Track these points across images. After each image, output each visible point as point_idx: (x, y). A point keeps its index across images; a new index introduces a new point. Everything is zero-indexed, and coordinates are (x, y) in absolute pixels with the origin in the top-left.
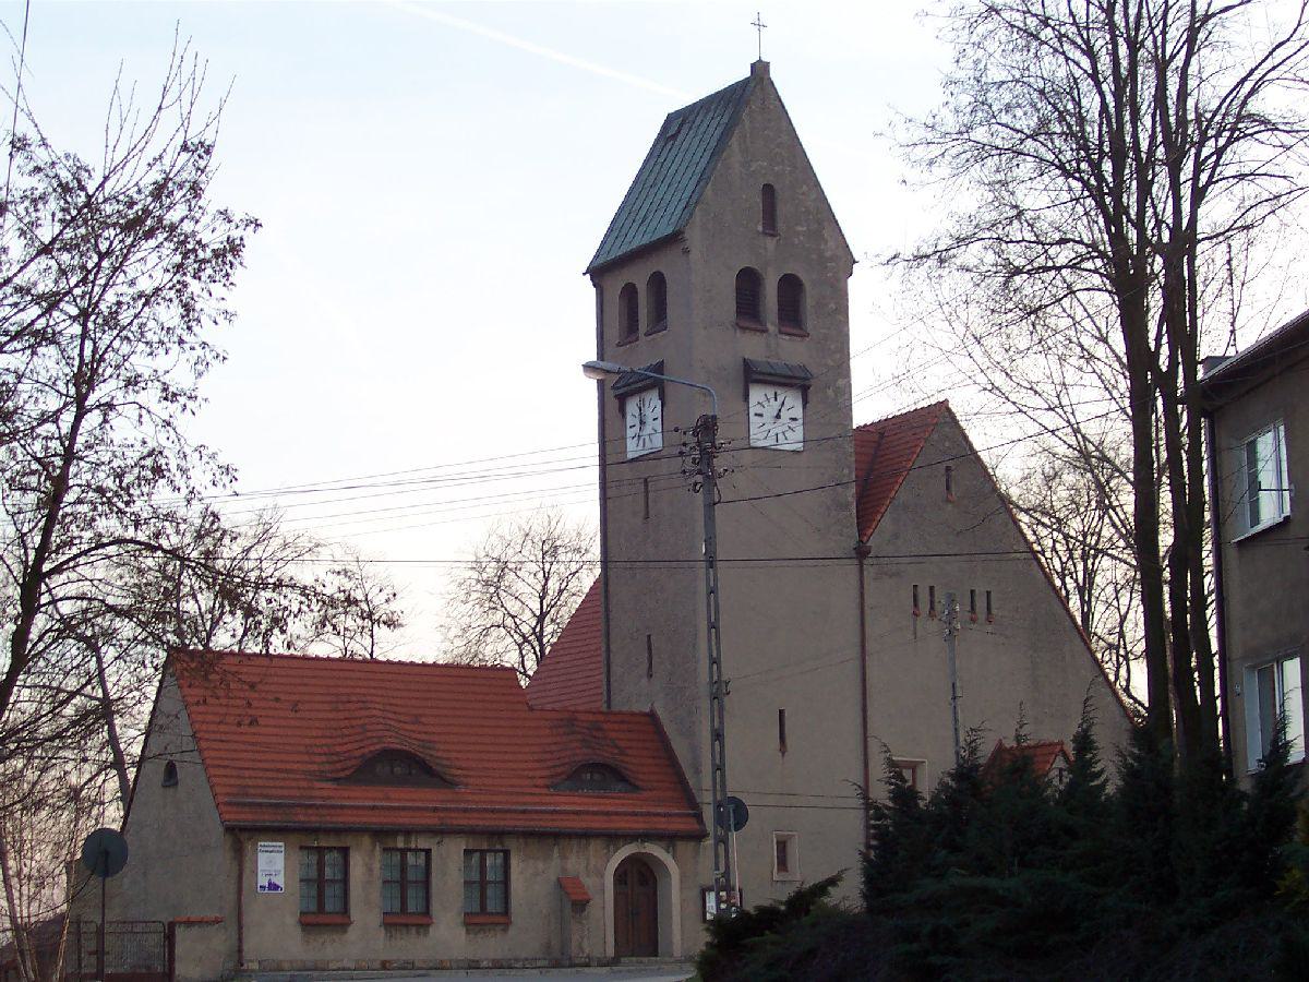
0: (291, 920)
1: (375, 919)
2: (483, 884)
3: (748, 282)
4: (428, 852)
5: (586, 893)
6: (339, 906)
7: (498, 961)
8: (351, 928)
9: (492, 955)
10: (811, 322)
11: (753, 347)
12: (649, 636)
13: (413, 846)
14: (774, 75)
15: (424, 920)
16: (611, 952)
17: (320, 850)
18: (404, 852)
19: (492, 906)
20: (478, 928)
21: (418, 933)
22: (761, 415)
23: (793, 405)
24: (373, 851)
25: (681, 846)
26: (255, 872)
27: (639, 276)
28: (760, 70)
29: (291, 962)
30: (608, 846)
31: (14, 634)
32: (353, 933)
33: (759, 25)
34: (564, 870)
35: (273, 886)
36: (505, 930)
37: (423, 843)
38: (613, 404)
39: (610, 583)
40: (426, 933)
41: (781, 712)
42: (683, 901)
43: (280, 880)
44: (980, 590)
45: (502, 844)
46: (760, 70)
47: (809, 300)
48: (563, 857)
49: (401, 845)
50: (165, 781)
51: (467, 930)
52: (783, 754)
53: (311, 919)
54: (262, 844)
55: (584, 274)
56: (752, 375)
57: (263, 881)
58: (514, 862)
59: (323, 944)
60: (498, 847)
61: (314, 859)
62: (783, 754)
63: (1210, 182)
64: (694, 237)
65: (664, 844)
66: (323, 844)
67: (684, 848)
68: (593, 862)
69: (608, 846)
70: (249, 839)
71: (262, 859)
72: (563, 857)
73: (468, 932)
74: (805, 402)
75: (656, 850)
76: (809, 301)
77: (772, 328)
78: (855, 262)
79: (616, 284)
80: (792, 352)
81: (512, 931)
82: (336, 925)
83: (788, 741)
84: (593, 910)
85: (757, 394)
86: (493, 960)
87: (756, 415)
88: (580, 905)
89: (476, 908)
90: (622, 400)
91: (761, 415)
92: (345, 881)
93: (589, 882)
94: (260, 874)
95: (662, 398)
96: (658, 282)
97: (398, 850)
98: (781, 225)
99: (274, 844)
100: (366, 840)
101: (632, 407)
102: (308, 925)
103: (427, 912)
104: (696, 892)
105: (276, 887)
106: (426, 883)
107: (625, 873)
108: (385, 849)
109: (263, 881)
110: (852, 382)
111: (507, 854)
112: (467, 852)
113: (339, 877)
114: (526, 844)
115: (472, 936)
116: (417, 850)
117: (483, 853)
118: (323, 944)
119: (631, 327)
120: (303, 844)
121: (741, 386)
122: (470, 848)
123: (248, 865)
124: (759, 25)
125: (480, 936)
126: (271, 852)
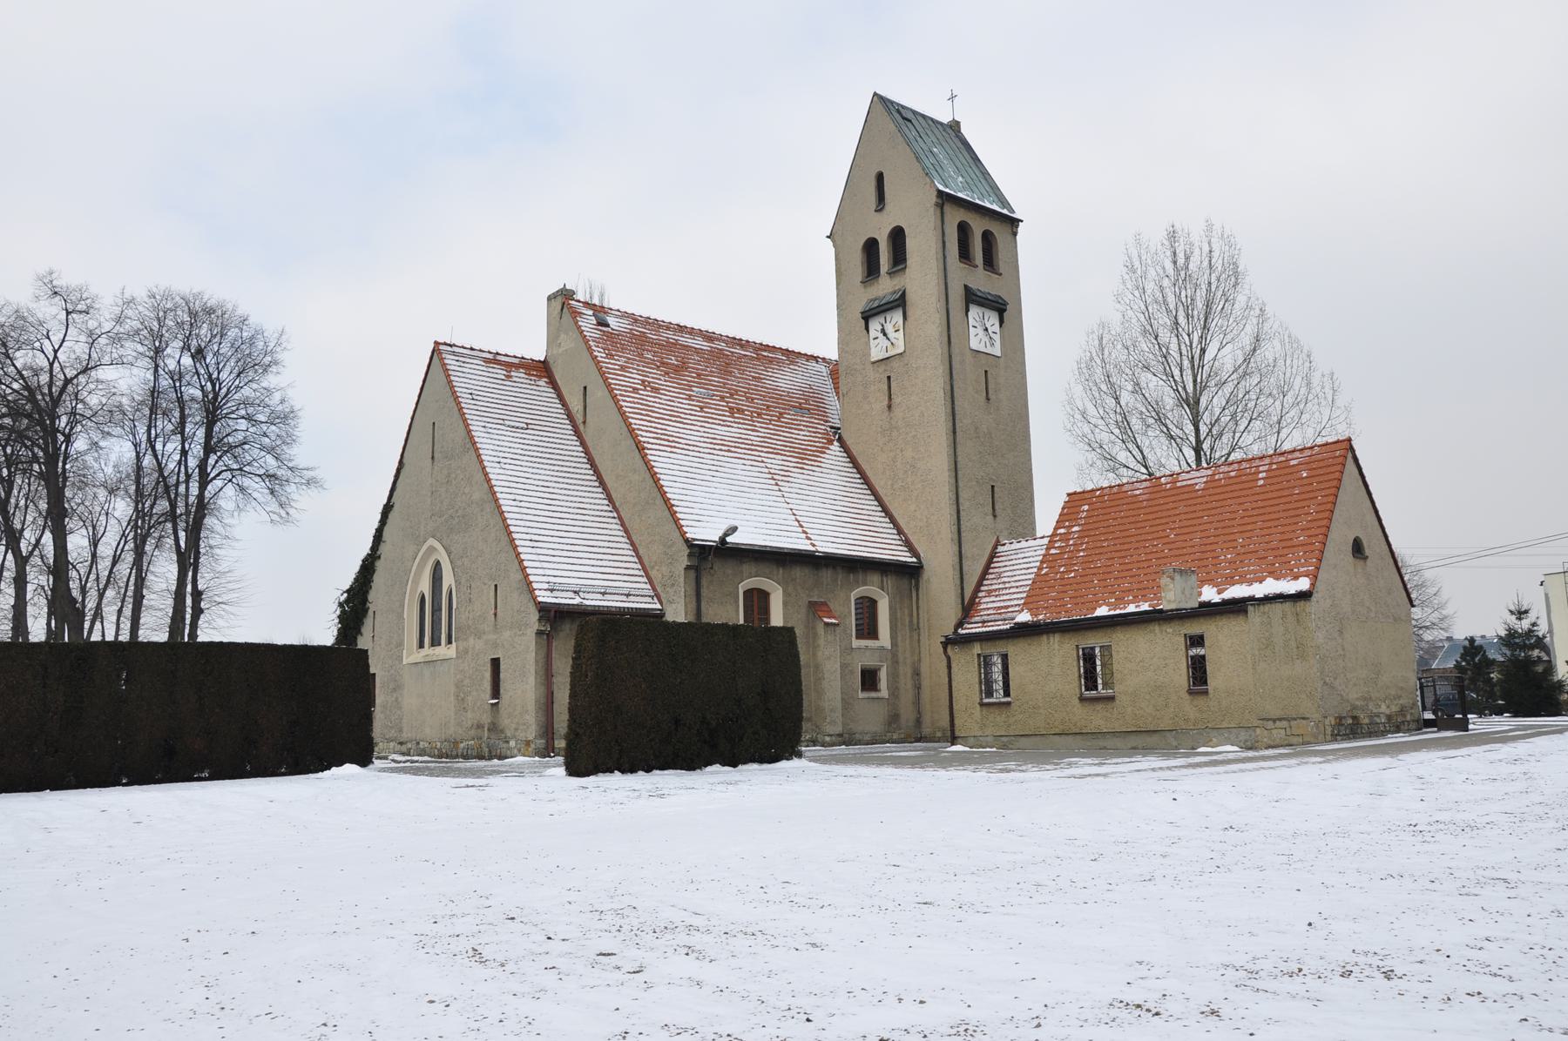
22: (976, 327)
23: (992, 320)
74: (1001, 322)
85: (975, 311)
91: (976, 327)
101: (875, 325)
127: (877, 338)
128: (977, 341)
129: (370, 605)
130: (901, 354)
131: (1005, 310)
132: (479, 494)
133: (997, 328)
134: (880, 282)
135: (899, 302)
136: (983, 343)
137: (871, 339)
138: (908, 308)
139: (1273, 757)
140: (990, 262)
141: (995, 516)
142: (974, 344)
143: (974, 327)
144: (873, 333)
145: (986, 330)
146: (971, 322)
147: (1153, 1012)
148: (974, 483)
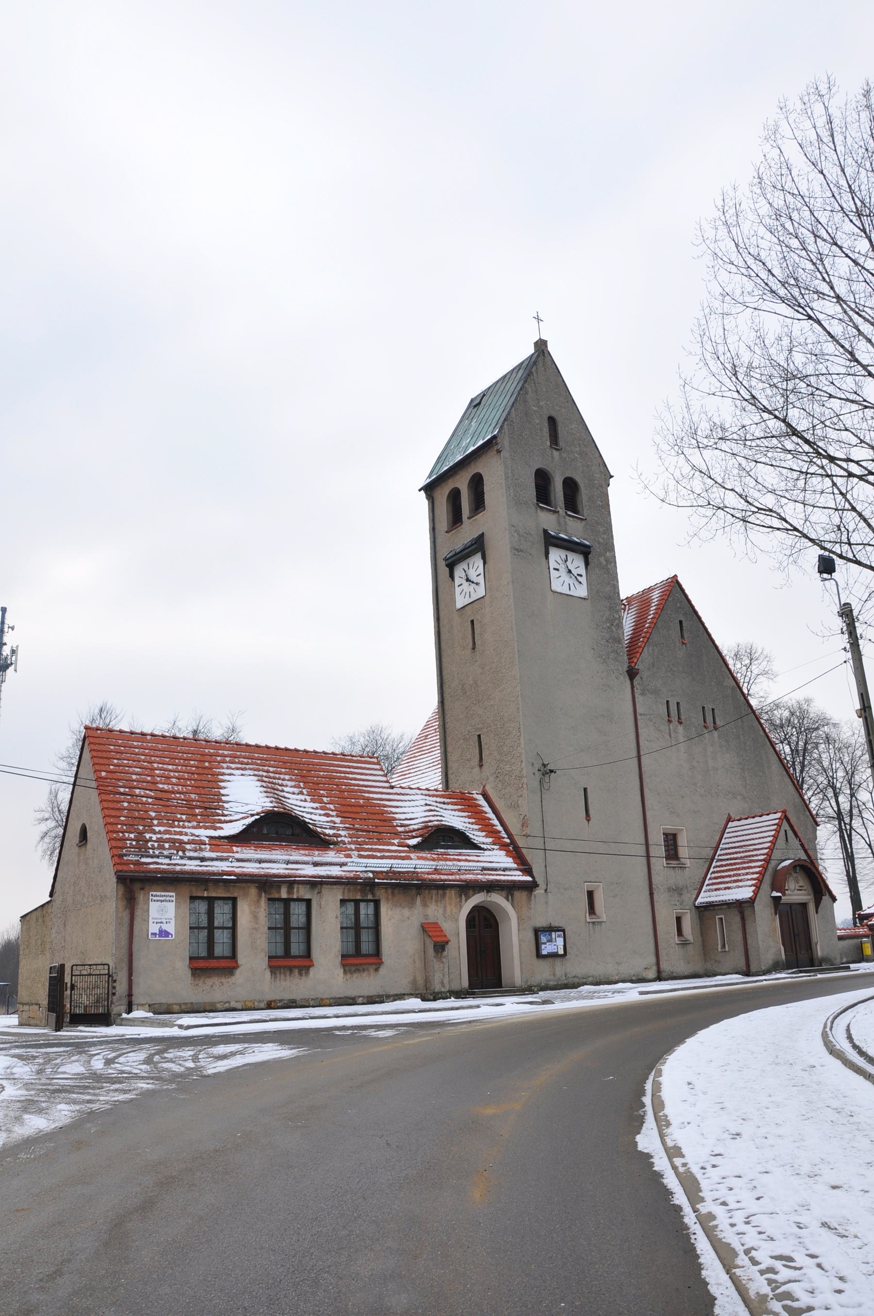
0: (182, 967)
1: (262, 962)
2: (357, 927)
3: (542, 479)
4: (308, 902)
5: (446, 936)
6: (227, 952)
7: (371, 997)
8: (238, 972)
9: (366, 994)
10: (586, 512)
11: (548, 521)
12: (479, 736)
13: (295, 897)
14: (551, 348)
15: (305, 962)
16: (465, 983)
17: (211, 901)
18: (287, 902)
19: (296, 949)
20: (353, 969)
21: (301, 974)
22: (558, 570)
23: (576, 563)
24: (258, 901)
25: (517, 894)
26: (147, 921)
27: (462, 483)
28: (541, 346)
29: (180, 1005)
30: (461, 896)
31: (639, 1133)
32: (239, 976)
33: (538, 319)
34: (426, 916)
35: (164, 933)
36: (377, 970)
37: (303, 892)
38: (444, 570)
39: (445, 701)
40: (307, 973)
41: (585, 790)
42: (520, 941)
43: (171, 928)
44: (709, 707)
45: (373, 894)
46: (541, 346)
47: (584, 496)
48: (425, 905)
49: (284, 895)
50: (80, 842)
51: (345, 971)
52: (588, 820)
53: (202, 964)
54: (154, 893)
55: (420, 490)
56: (551, 541)
57: (154, 928)
58: (384, 909)
59: (212, 986)
60: (370, 897)
61: (203, 907)
62: (588, 820)
63: (826, 452)
64: (505, 442)
65: (504, 893)
66: (214, 895)
67: (519, 895)
68: (448, 909)
69: (461, 896)
70: (142, 889)
71: (154, 908)
72: (425, 905)
73: (345, 972)
74: (587, 564)
75: (498, 899)
76: (584, 494)
77: (562, 511)
78: (612, 477)
79: (443, 495)
80: (575, 530)
81: (383, 971)
82: (224, 969)
83: (591, 812)
84: (451, 949)
85: (556, 555)
86: (368, 997)
87: (555, 569)
88: (440, 947)
89: (280, 951)
90: (451, 566)
91: (558, 570)
92: (234, 929)
93: (447, 927)
94: (151, 921)
95: (484, 558)
96: (477, 483)
97: (280, 900)
98: (561, 443)
99: (167, 894)
100: (253, 891)
101: (459, 572)
102: (196, 969)
103: (308, 955)
104: (531, 935)
105: (167, 934)
106: (307, 928)
107: (474, 917)
108: (269, 899)
109: (154, 928)
110: (616, 555)
111: (377, 904)
112: (343, 902)
113: (230, 925)
114: (393, 893)
115: (349, 976)
116: (298, 900)
117: (357, 903)
118: (212, 986)
119: (456, 519)
120: (194, 895)
121: (545, 547)
122: (346, 898)
123: (138, 913)
124: (538, 319)
125: (355, 975)
126: (162, 901)
127: (461, 585)
128: (560, 583)
129: (202, 980)
130: (483, 597)
131: (589, 553)
132: (597, 455)
133: (582, 571)
134: (63, 765)
135: (478, 546)
136: (566, 585)
137: (456, 585)
138: (489, 553)
139: (300, 863)
140: (572, 503)
141: (481, 766)
142: (556, 586)
143: (555, 569)
144: (457, 581)
145: (570, 571)
146: (552, 564)
147: (762, 1267)
148: (462, 741)
